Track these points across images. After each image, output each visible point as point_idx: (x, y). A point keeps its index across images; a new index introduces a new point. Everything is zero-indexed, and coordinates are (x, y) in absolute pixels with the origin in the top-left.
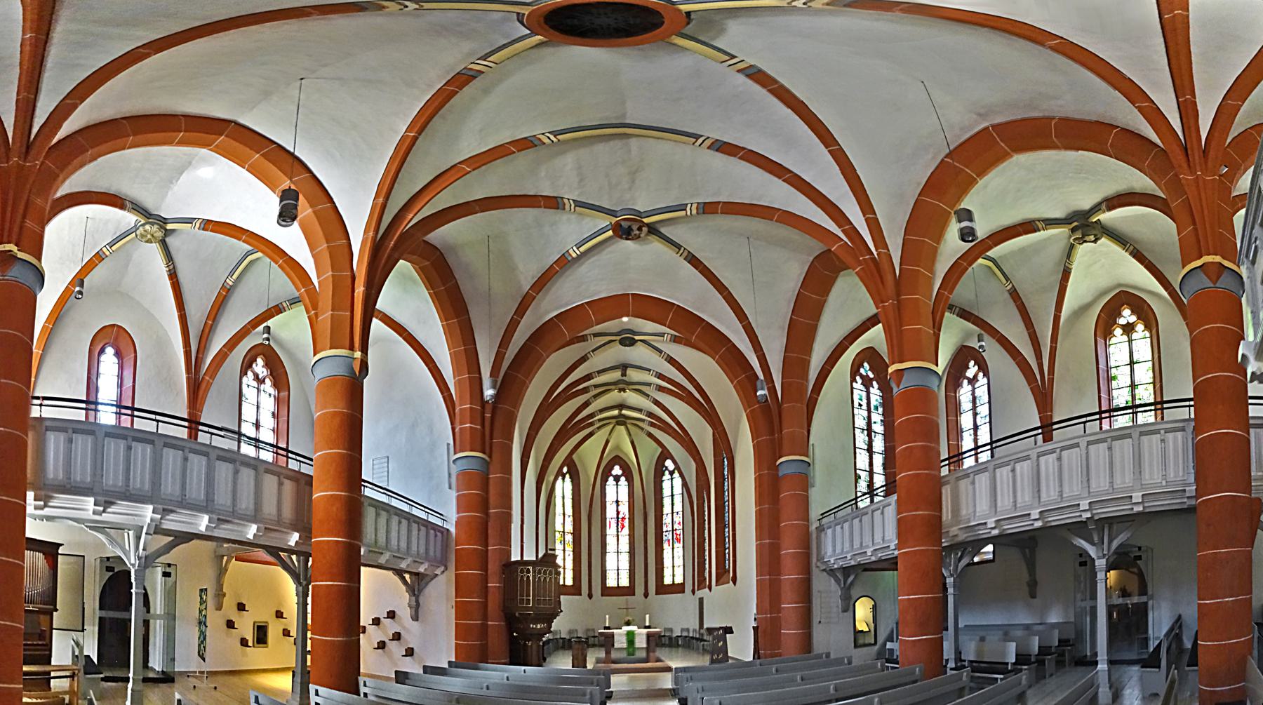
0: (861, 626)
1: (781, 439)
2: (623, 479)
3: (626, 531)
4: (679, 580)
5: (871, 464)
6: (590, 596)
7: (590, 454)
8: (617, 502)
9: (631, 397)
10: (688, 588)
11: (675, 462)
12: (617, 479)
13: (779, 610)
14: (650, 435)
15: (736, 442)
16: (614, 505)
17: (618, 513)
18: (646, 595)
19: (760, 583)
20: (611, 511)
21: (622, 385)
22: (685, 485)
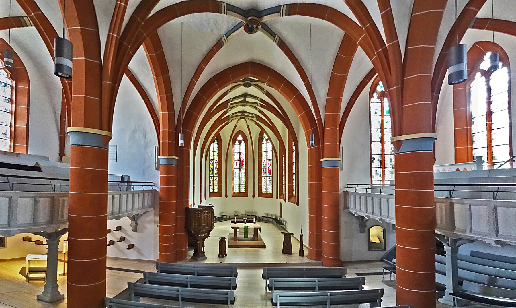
0: (374, 239)
2: (243, 142)
3: (244, 167)
4: (270, 191)
5: (383, 150)
6: (226, 197)
7: (226, 132)
8: (240, 153)
9: (248, 109)
10: (274, 195)
12: (240, 142)
13: (321, 231)
14: (257, 124)
15: (298, 134)
16: (238, 155)
17: (240, 158)
18: (254, 197)
20: (237, 157)
21: (244, 103)
22: (273, 147)
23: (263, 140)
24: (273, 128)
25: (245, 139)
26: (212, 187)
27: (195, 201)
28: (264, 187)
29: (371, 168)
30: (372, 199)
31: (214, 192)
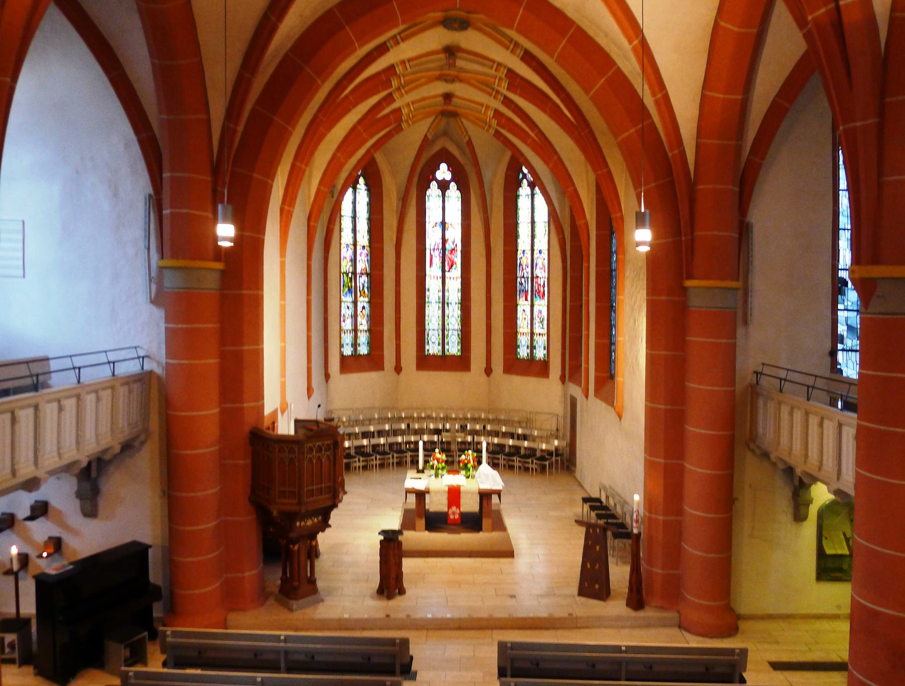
1: (692, 240)
2: (453, 186)
4: (540, 354)
6: (398, 369)
11: (532, 171)
12: (444, 186)
16: (439, 230)
18: (488, 371)
19: (651, 413)
20: (433, 237)
23: (519, 185)
24: (545, 148)
25: (460, 178)
26: (347, 339)
27: (285, 394)
28: (523, 341)
29: (835, 310)
30: (821, 425)
31: (355, 356)
